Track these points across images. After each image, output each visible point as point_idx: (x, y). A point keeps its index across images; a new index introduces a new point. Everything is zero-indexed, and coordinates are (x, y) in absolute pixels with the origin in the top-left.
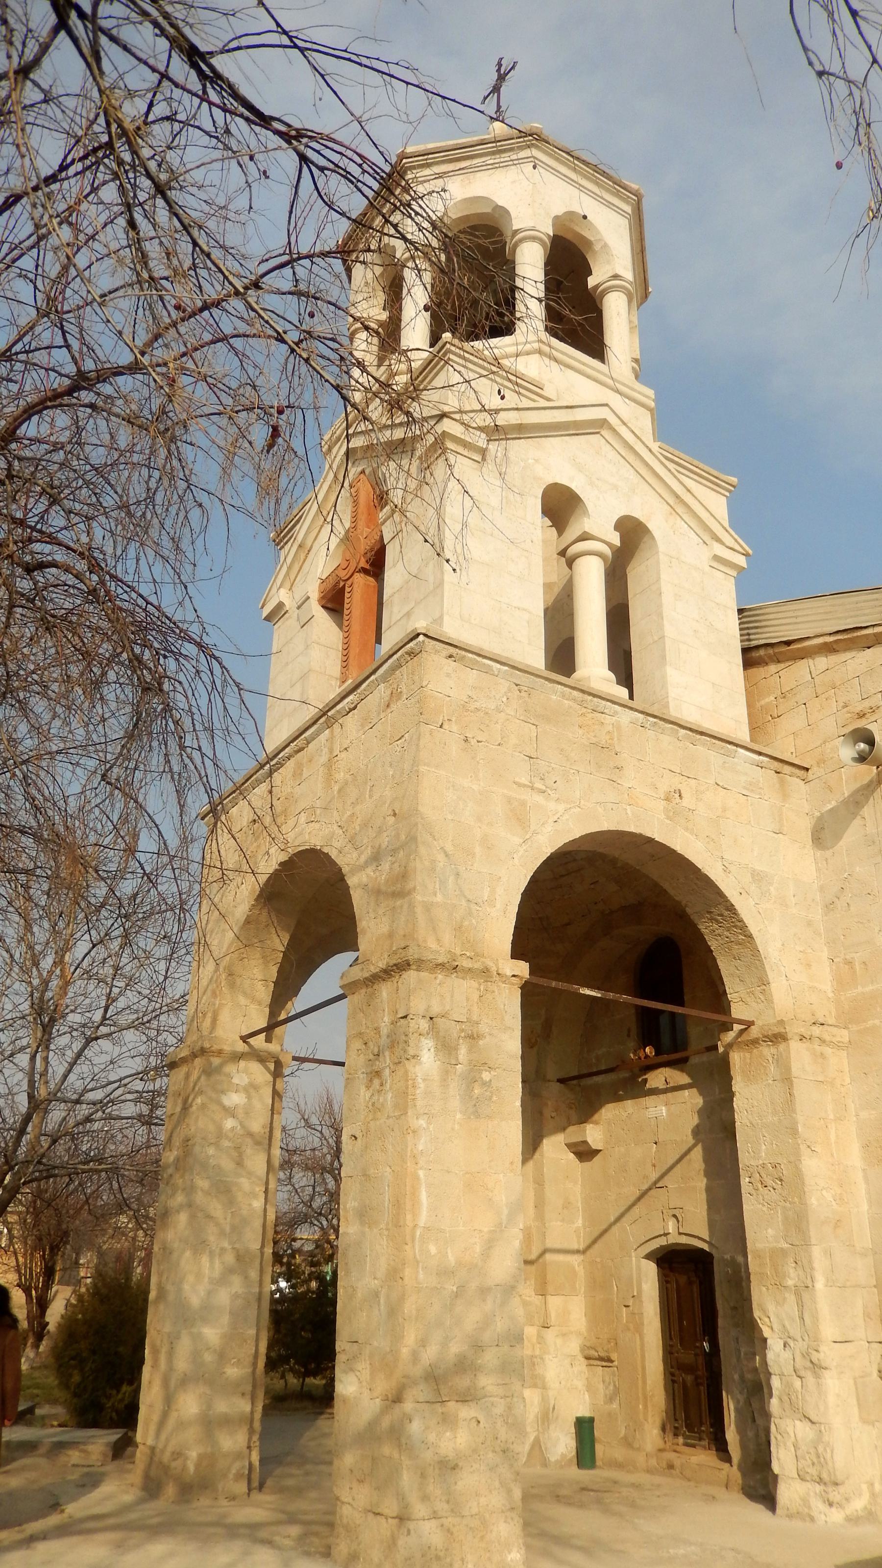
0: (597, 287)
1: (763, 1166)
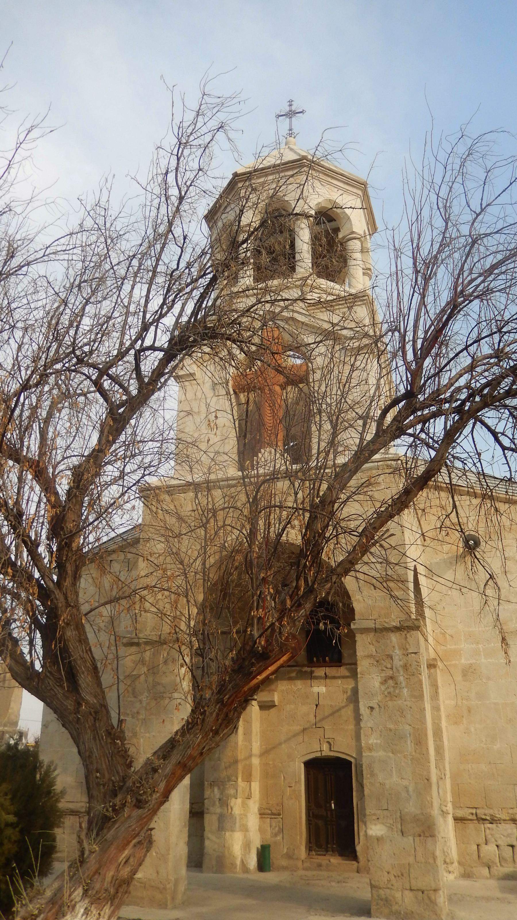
0: (344, 238)
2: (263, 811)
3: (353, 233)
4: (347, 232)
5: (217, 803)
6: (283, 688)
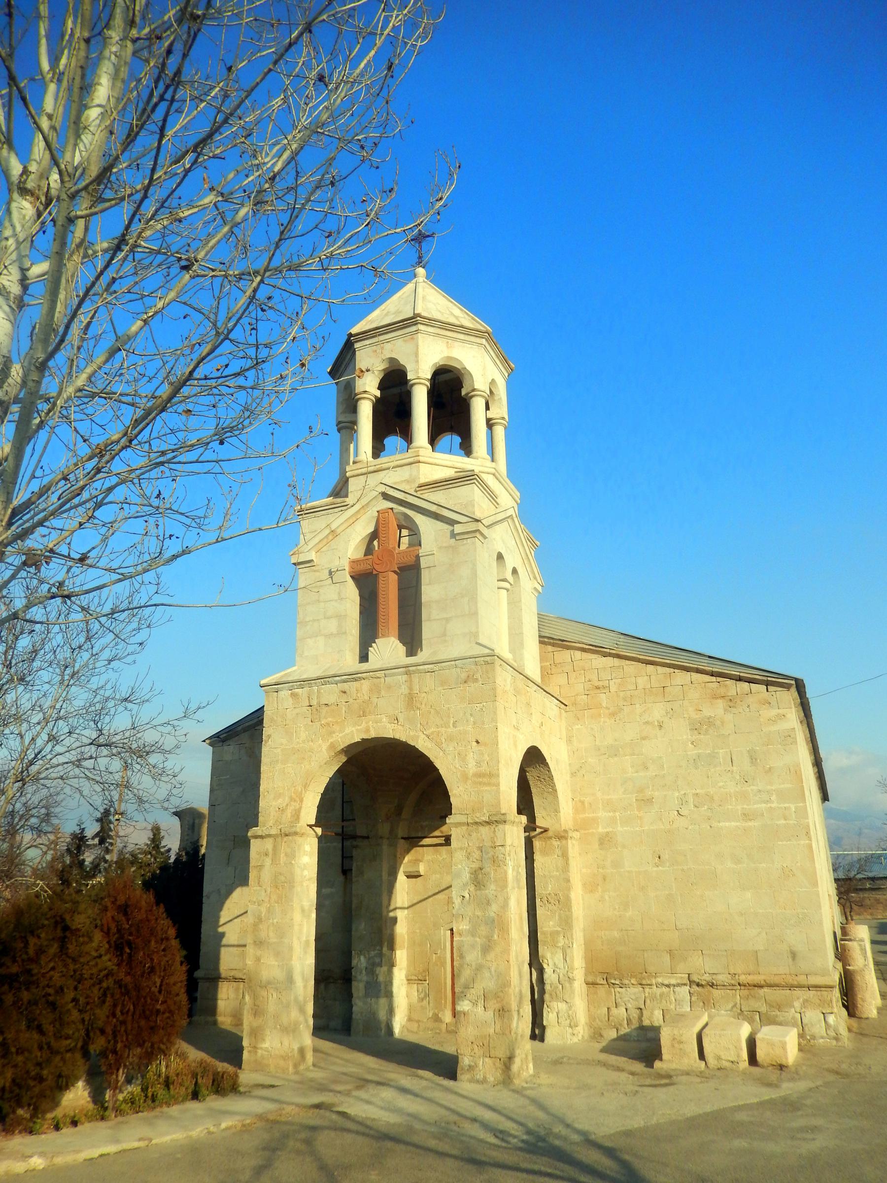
0: (467, 394)
1: (550, 894)
2: (410, 978)
3: (474, 390)
4: (470, 389)
5: (364, 972)
6: (430, 858)
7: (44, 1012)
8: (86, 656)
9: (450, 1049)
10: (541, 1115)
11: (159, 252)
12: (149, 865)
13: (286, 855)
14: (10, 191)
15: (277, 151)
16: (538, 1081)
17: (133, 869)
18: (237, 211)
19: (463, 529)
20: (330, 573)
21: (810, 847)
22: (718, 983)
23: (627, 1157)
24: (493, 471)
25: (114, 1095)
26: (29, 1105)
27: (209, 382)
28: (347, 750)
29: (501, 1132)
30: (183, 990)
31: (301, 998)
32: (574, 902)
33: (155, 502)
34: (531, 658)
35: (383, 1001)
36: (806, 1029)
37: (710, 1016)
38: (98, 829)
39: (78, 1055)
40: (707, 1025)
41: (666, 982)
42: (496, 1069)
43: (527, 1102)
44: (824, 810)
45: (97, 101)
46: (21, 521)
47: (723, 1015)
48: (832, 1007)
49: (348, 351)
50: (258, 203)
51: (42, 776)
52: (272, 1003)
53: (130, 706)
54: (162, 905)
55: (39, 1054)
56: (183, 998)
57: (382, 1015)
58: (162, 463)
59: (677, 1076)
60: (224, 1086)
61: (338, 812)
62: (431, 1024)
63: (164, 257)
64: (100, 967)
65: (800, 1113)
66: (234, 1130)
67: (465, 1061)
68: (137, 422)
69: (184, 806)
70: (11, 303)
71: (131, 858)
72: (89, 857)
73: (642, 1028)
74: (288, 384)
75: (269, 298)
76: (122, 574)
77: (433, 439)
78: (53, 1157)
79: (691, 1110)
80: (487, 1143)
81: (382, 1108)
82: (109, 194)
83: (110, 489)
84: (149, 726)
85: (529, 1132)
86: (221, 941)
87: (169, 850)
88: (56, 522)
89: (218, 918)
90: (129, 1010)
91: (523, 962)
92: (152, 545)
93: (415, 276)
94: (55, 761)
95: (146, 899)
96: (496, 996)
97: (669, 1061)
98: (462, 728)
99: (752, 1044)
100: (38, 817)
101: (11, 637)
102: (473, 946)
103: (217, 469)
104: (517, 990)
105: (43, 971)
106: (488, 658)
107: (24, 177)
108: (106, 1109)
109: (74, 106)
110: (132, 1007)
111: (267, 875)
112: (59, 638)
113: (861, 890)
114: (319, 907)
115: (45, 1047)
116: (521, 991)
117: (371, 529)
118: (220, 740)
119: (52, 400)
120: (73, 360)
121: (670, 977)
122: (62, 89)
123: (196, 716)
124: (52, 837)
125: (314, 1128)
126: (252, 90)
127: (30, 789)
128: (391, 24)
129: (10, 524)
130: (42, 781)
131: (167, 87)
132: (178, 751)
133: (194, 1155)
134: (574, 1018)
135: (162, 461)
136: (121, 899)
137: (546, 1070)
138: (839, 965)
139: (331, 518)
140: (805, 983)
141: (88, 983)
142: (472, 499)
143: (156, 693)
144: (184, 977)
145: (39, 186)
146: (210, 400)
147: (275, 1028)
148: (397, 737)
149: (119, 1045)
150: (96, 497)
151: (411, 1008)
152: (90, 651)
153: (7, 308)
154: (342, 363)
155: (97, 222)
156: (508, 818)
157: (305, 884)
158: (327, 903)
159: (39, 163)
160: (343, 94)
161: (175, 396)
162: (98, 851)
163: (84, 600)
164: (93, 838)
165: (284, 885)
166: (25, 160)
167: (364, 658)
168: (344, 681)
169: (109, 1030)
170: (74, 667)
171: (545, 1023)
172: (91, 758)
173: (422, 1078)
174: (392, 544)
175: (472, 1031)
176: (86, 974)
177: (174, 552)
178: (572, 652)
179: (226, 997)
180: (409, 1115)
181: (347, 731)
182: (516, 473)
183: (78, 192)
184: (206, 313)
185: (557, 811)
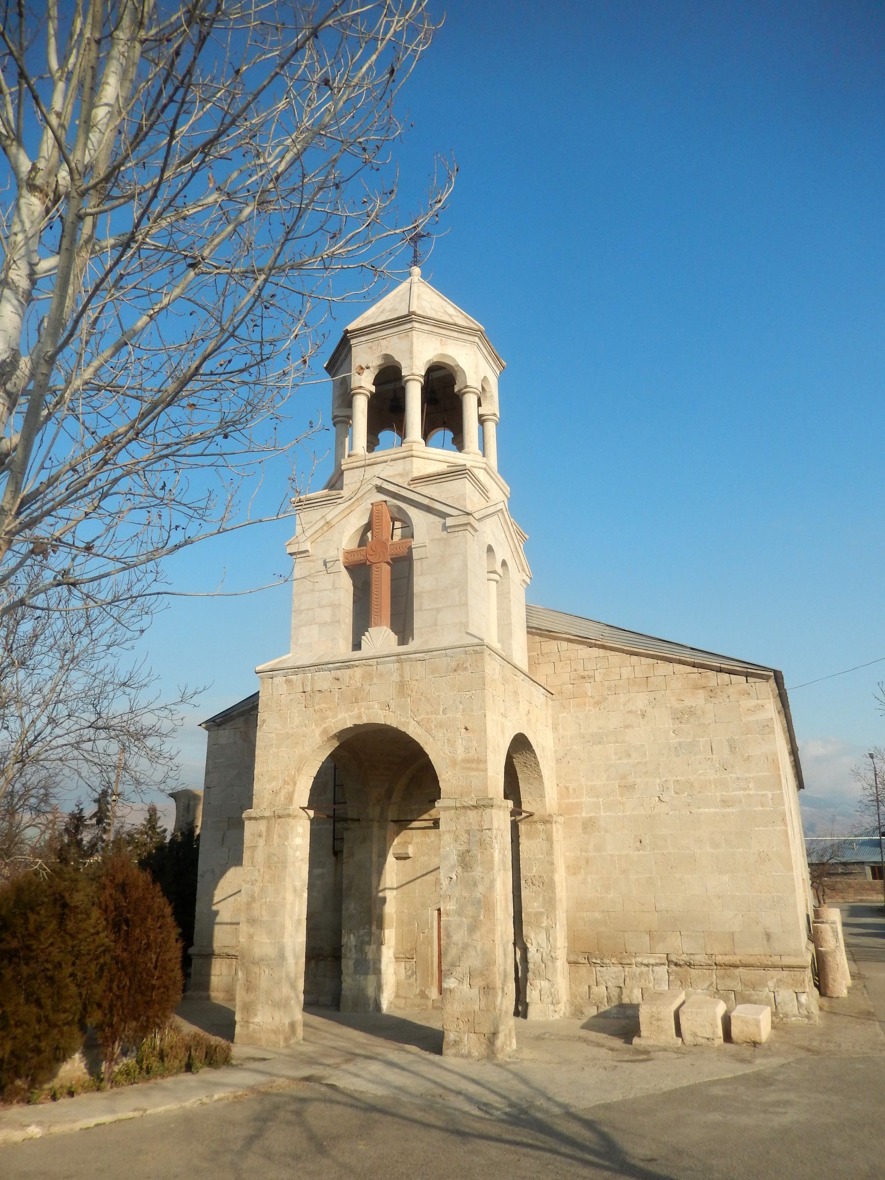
2: (398, 956)
3: (466, 387)
4: (463, 386)
7: (43, 986)
8: (85, 641)
9: (436, 1025)
10: (523, 1088)
11: (166, 250)
12: (145, 844)
13: (279, 836)
14: (19, 187)
15: (280, 151)
16: (521, 1056)
17: (130, 848)
18: (241, 211)
19: (454, 522)
20: (325, 563)
21: (786, 832)
22: (696, 963)
23: (606, 1129)
24: (484, 466)
25: (110, 1067)
26: (27, 1076)
27: (213, 378)
28: (340, 735)
29: (485, 1104)
30: (178, 966)
31: (292, 975)
32: (557, 884)
33: (160, 494)
34: (519, 648)
35: (371, 978)
36: (779, 1007)
37: (687, 995)
38: (96, 809)
39: (75, 1029)
40: (684, 1003)
41: (645, 962)
42: (481, 1044)
43: (511, 1076)
44: (800, 797)
45: (104, 100)
46: (29, 511)
47: (699, 994)
48: (805, 987)
49: (344, 347)
50: (263, 203)
51: (42, 757)
52: (264, 979)
53: (128, 690)
54: (158, 884)
55: (37, 1027)
56: (178, 974)
57: (371, 991)
58: (167, 456)
59: (655, 1051)
60: (216, 1059)
61: (330, 795)
62: (417, 1001)
63: (172, 254)
64: (97, 943)
65: (773, 1088)
66: (226, 1101)
67: (451, 1036)
68: (143, 416)
69: (180, 788)
70: (20, 297)
71: (128, 838)
72: (86, 837)
73: (621, 1006)
74: (289, 381)
75: (273, 296)
76: (124, 563)
77: (425, 435)
78: (50, 1127)
79: (667, 1085)
80: (471, 1115)
81: (370, 1081)
82: (115, 192)
83: (116, 481)
84: (146, 710)
85: (512, 1105)
86: (215, 919)
87: (165, 831)
88: (61, 512)
89: (212, 896)
90: (125, 985)
91: (508, 942)
92: (156, 535)
93: (410, 275)
94: (54, 743)
95: (143, 878)
96: (482, 974)
97: (647, 1037)
98: (451, 715)
99: (727, 1022)
100: (37, 797)
101: (12, 622)
102: (460, 926)
103: (221, 462)
104: (502, 968)
105: (42, 947)
106: (478, 648)
107: (33, 174)
108: (102, 1080)
109: (85, 106)
110: (128, 982)
111: (260, 855)
112: (60, 623)
113: (833, 874)
114: (311, 887)
115: (43, 1020)
116: (505, 969)
117: (365, 521)
118: (215, 724)
119: (59, 393)
120: (81, 354)
121: (649, 957)
122: (71, 88)
123: (192, 701)
124: (50, 817)
125: (304, 1100)
126: (259, 93)
127: (29, 769)
128: (392, 30)
129: (18, 513)
130: (41, 762)
131: (177, 89)
132: (174, 735)
133: (187, 1125)
134: (556, 996)
135: (168, 453)
136: (120, 878)
137: (527, 1042)
138: (812, 946)
139: (327, 510)
140: (779, 963)
141: (85, 959)
142: (463, 493)
143: (154, 677)
144: (179, 954)
145: (48, 183)
146: (216, 394)
147: (267, 1003)
148: (388, 723)
149: (115, 1019)
150: (102, 487)
151: (398, 985)
152: (90, 636)
153: (15, 302)
154: (338, 359)
155: (108, 218)
156: (495, 802)
157: (297, 865)
158: (318, 883)
159: (48, 160)
160: (345, 98)
161: (181, 390)
162: (96, 831)
163: (85, 588)
164: (91, 818)
165: (277, 864)
166: (34, 155)
167: (357, 646)
168: (338, 669)
169: (106, 1004)
170: (73, 651)
171: (528, 1000)
172: (90, 740)
173: (409, 1052)
174: (386, 535)
175: (458, 1008)
176: (84, 949)
177: (177, 542)
178: (559, 642)
179: (220, 973)
180: (396, 1088)
181: (340, 716)
182: (507, 468)
183: (88, 189)
184: (211, 310)
185: (542, 796)
